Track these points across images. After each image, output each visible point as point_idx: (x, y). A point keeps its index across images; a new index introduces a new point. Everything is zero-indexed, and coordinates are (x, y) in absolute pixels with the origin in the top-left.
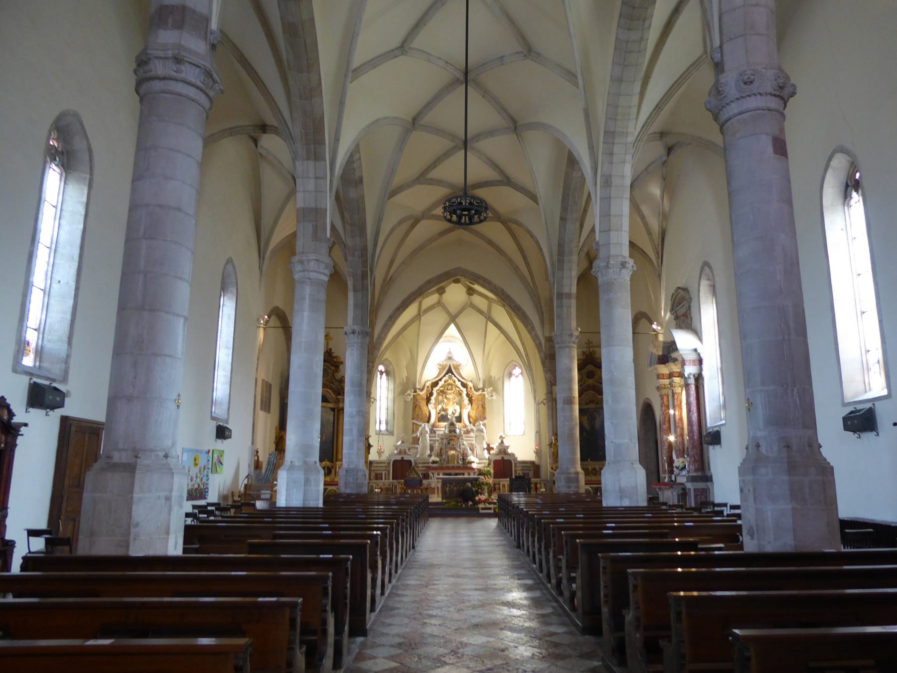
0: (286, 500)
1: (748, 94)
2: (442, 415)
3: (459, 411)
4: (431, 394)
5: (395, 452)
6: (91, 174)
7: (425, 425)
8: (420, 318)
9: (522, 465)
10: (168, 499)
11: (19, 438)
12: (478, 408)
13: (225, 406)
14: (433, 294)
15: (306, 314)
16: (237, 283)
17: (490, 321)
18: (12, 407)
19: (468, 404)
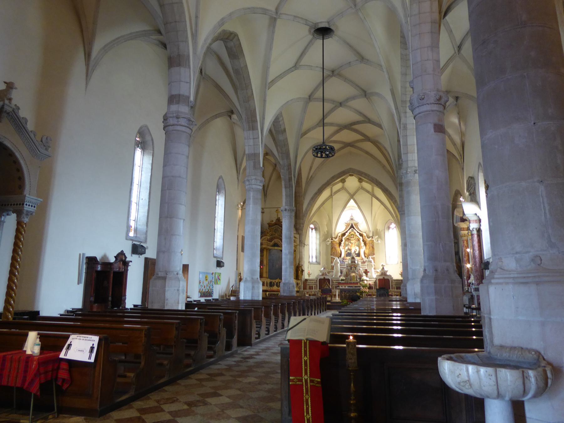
0: (244, 297)
1: (422, 104)
2: (348, 253)
3: (358, 250)
4: (342, 240)
5: (320, 274)
6: (153, 151)
7: (337, 259)
8: (332, 197)
10: (178, 290)
11: (129, 267)
12: (370, 248)
13: (221, 251)
14: (339, 183)
15: (251, 206)
16: (225, 188)
17: (374, 197)
18: (126, 255)
19: (364, 246)
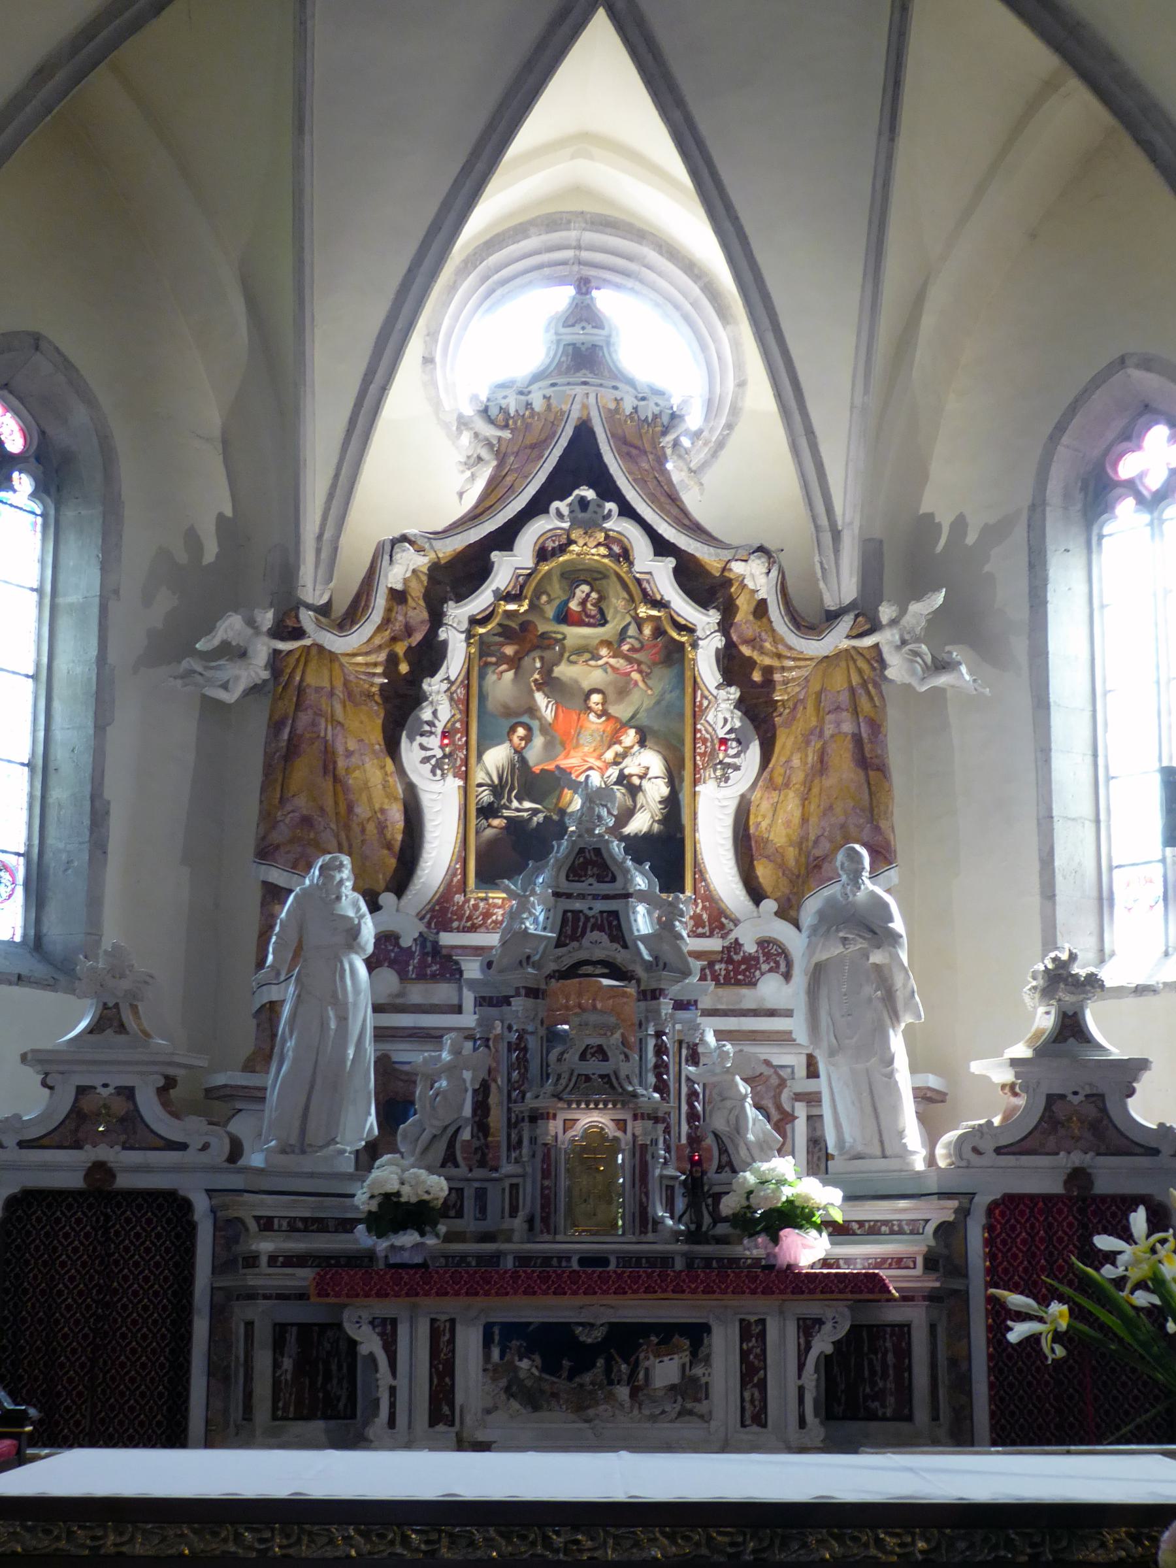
2: (515, 826)
9: (552, 1196)
12: (822, 766)
